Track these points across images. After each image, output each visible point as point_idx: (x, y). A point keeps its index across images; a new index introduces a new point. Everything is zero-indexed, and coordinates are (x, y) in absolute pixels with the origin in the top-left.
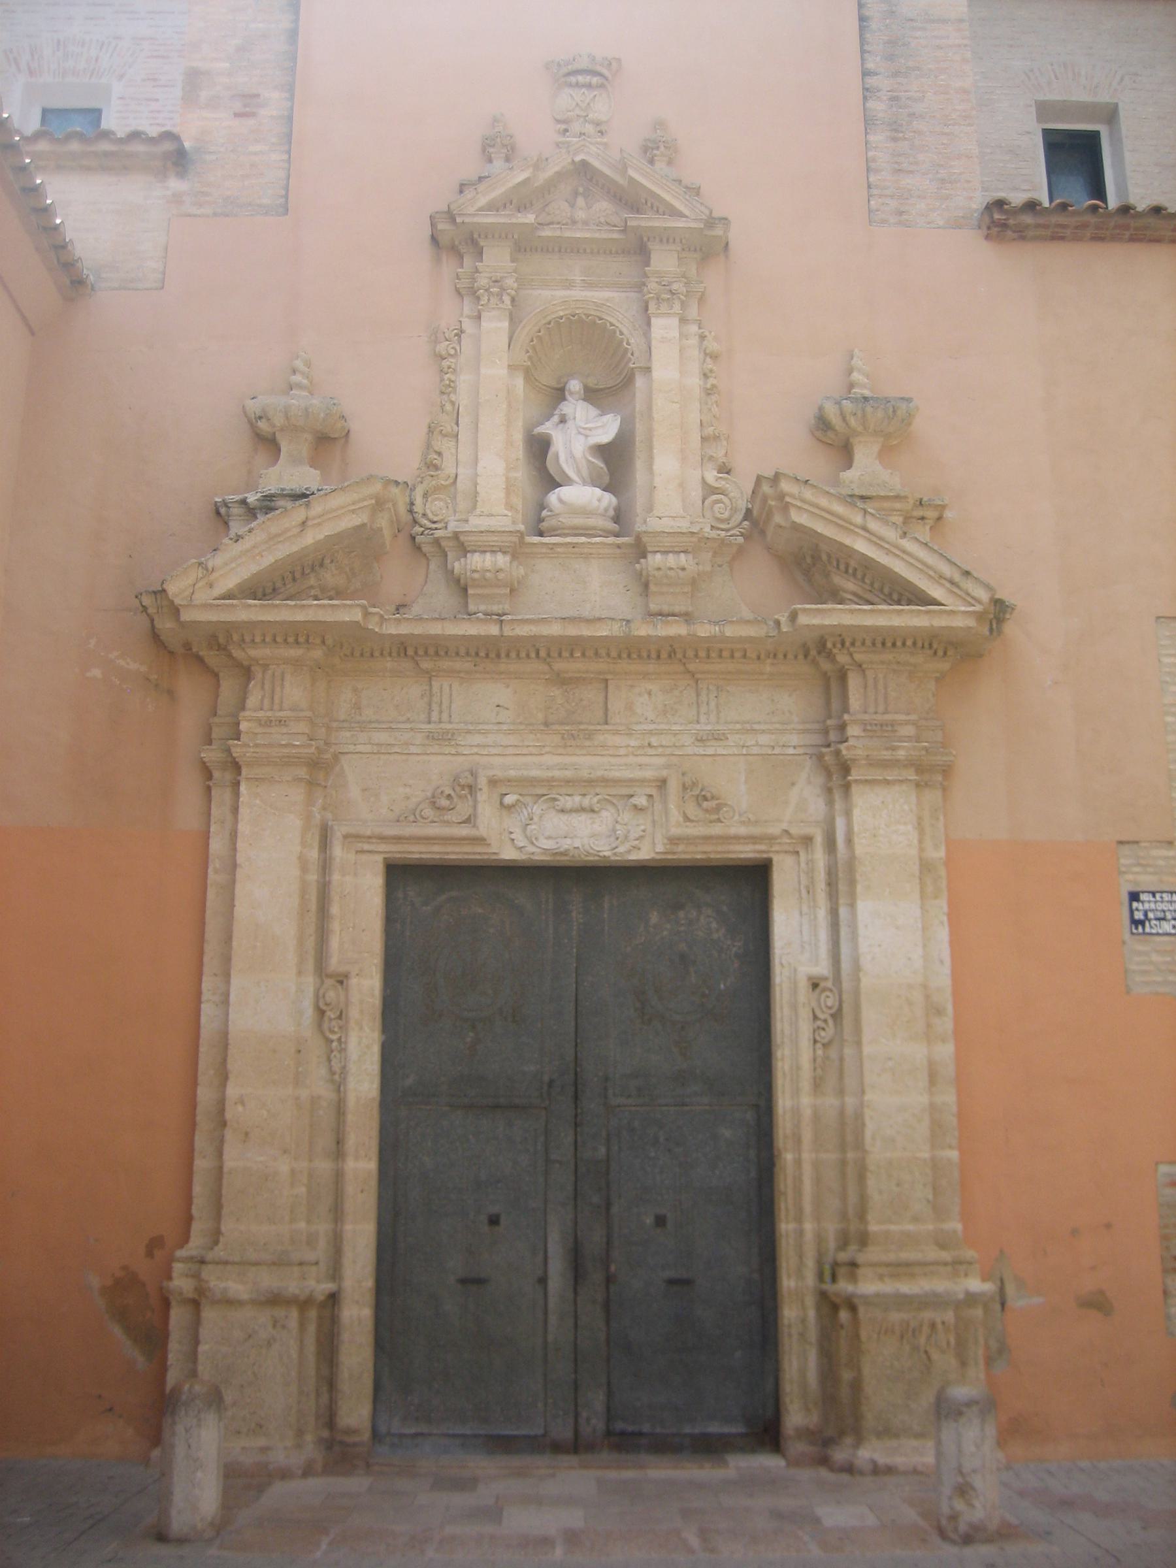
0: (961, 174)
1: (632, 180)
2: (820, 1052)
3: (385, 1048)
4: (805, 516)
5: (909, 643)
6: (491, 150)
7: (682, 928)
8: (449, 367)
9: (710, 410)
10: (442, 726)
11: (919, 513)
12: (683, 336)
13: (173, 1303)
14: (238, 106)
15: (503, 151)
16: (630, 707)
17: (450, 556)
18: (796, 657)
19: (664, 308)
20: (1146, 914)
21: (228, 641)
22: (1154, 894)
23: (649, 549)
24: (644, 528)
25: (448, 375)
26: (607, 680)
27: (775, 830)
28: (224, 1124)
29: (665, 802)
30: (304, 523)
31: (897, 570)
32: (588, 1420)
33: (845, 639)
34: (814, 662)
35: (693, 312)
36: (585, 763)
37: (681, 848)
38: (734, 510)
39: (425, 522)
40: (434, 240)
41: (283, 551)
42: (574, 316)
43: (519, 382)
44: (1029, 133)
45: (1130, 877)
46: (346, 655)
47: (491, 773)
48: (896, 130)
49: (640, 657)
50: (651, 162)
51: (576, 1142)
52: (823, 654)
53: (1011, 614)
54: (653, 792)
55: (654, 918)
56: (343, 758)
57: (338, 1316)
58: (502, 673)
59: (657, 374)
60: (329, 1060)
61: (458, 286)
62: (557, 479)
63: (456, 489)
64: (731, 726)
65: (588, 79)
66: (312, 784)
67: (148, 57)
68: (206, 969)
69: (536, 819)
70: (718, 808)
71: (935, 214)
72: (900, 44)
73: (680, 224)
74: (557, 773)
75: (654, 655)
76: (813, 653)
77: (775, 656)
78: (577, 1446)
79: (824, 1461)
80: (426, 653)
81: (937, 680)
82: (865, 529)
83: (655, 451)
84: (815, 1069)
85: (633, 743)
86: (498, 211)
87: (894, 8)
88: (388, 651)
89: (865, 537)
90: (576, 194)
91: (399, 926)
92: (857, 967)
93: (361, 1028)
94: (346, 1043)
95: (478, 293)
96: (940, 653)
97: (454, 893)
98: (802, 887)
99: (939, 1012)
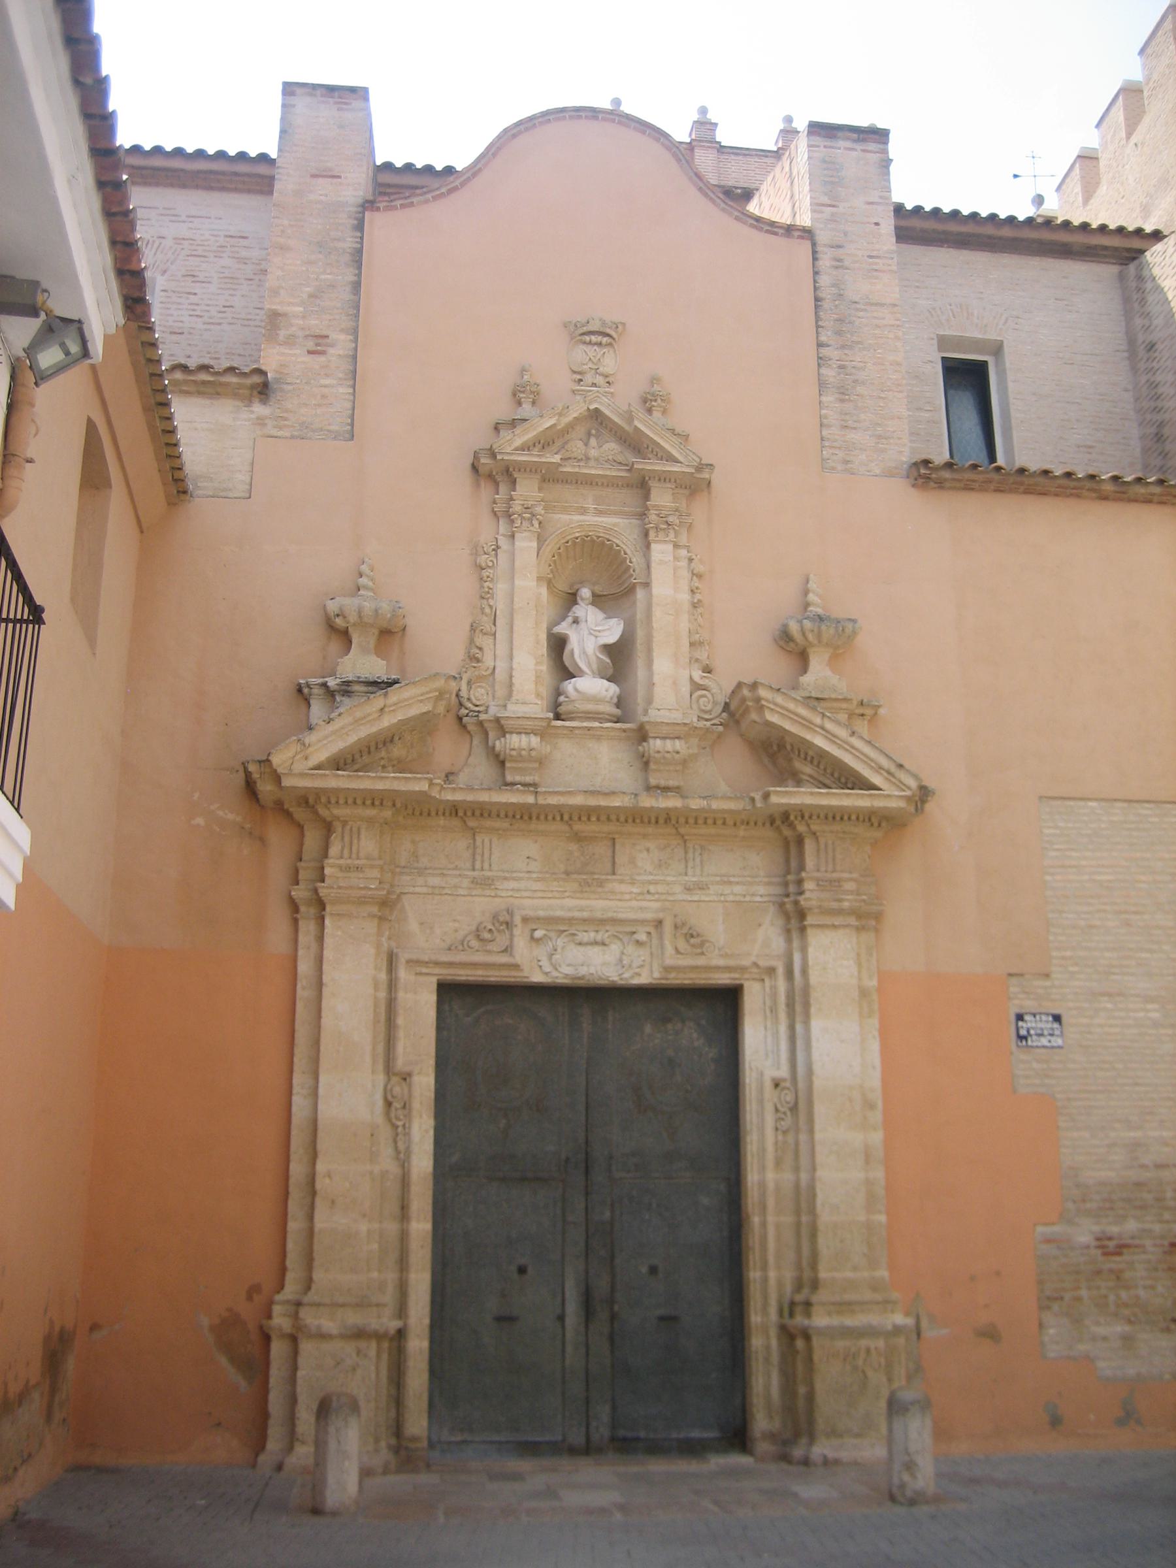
0: (894, 432)
1: (636, 429)
2: (780, 1137)
3: (436, 1129)
4: (776, 716)
5: (854, 817)
7: (670, 1037)
8: (488, 577)
9: (696, 620)
10: (483, 873)
12: (676, 558)
14: (310, 345)
15: (531, 396)
16: (632, 861)
17: (492, 735)
18: (764, 824)
19: (661, 536)
20: (1028, 1031)
21: (316, 802)
22: (1034, 1015)
23: (651, 735)
24: (645, 719)
25: (487, 583)
26: (614, 839)
27: (746, 962)
28: (314, 1193)
29: (661, 938)
30: (382, 709)
31: (846, 761)
33: (803, 813)
34: (778, 828)
35: (683, 539)
36: (598, 905)
37: (673, 975)
38: (715, 703)
39: (469, 705)
40: (475, 468)
41: (364, 732)
42: (587, 537)
43: (544, 591)
44: (932, 362)
45: (1016, 1002)
46: (408, 814)
47: (524, 913)
48: (843, 393)
49: (642, 822)
50: (649, 411)
51: (587, 1208)
52: (786, 824)
53: (932, 797)
54: (651, 930)
55: (648, 1029)
56: (404, 898)
57: (404, 1346)
58: (531, 831)
60: (395, 1142)
61: (495, 509)
62: (571, 669)
63: (494, 679)
64: (712, 879)
65: (599, 338)
66: (382, 919)
67: (188, 256)
68: (296, 1068)
69: (559, 950)
70: (702, 944)
71: (873, 464)
72: (847, 321)
73: (676, 468)
74: (577, 914)
75: (653, 820)
76: (778, 822)
77: (748, 823)
78: (588, 1449)
79: (785, 1458)
80: (473, 814)
82: (822, 728)
83: (654, 654)
84: (776, 1151)
85: (635, 890)
86: (529, 450)
87: (842, 291)
88: (442, 811)
89: (823, 735)
90: (589, 434)
93: (421, 1117)
94: (410, 1128)
95: (512, 517)
96: (876, 824)
98: (767, 1008)
99: (872, 1107)
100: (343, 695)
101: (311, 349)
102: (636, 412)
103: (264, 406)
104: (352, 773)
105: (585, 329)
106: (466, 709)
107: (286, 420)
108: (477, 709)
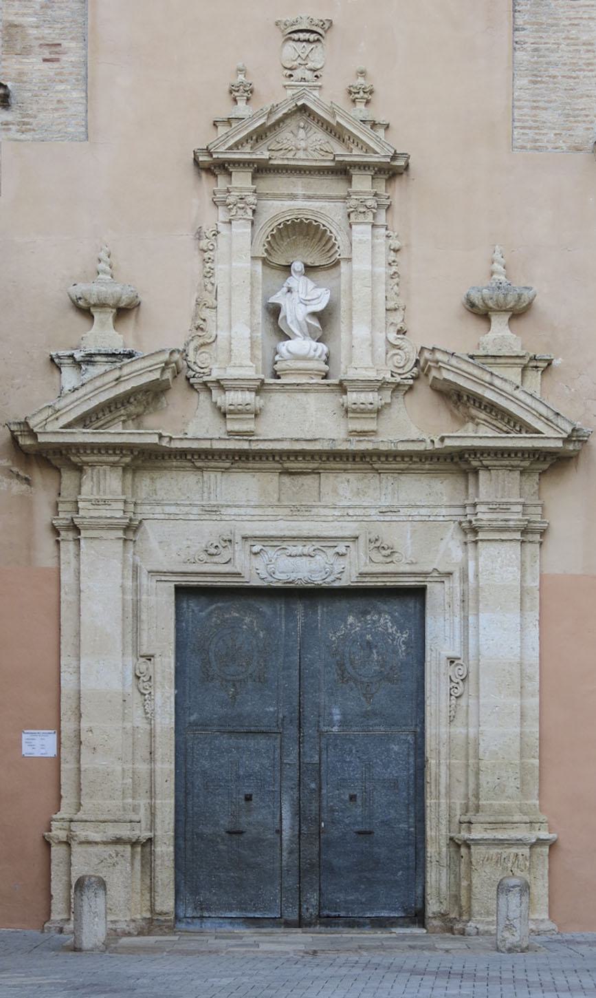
2: (453, 702)
3: (176, 697)
4: (452, 374)
6: (236, 94)
8: (209, 259)
11: (534, 364)
13: (53, 844)
16: (335, 491)
23: (349, 390)
27: (429, 569)
32: (307, 909)
36: (306, 527)
38: (408, 360)
40: (196, 161)
42: (297, 219)
55: (351, 619)
59: (356, 266)
78: (300, 923)
81: (540, 474)
85: (336, 514)
91: (184, 624)
92: (478, 653)
93: (163, 687)
97: (220, 605)
99: (531, 679)
100: (88, 364)
101: (48, 56)
102: (337, 108)
103: (7, 112)
104: (95, 431)
105: (295, 28)
106: (193, 371)
107: (27, 125)
108: (202, 371)
